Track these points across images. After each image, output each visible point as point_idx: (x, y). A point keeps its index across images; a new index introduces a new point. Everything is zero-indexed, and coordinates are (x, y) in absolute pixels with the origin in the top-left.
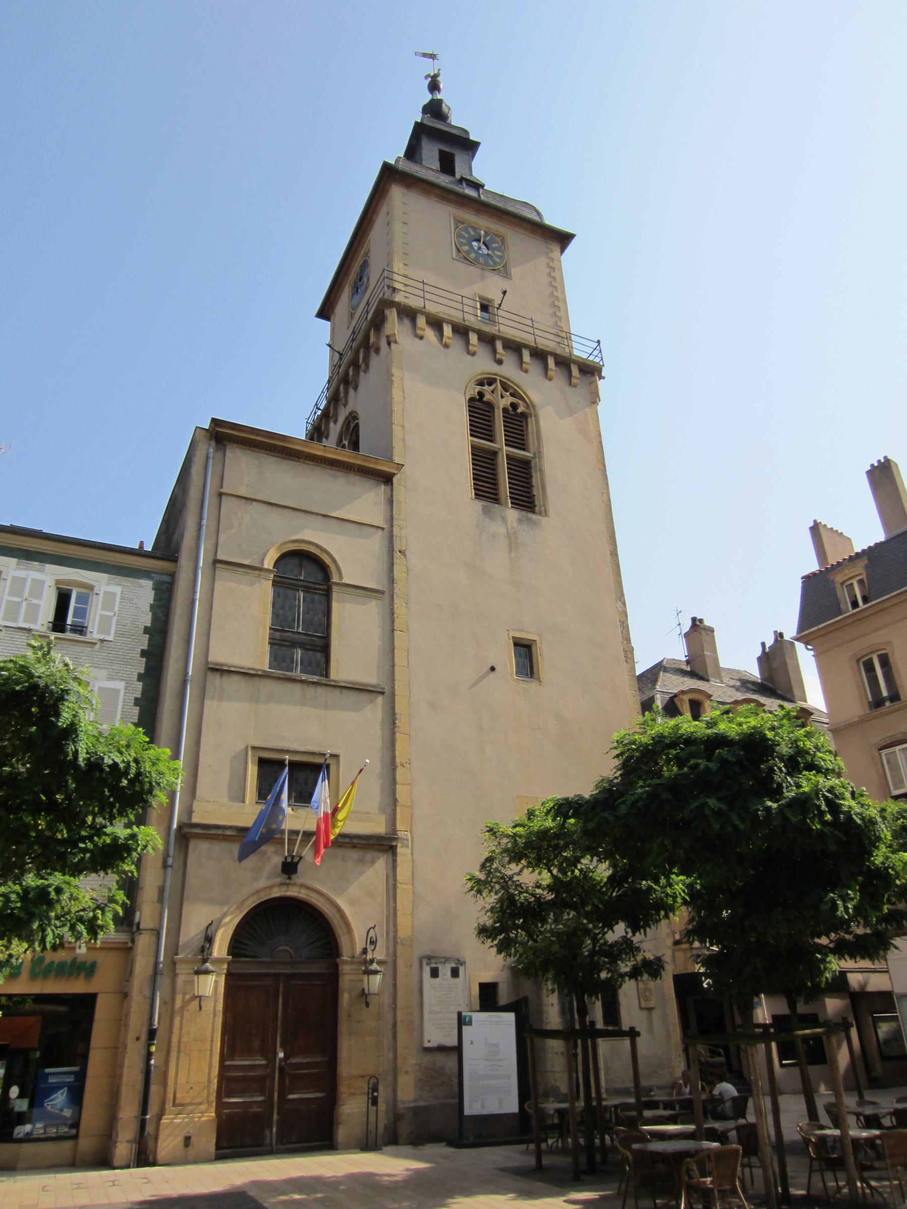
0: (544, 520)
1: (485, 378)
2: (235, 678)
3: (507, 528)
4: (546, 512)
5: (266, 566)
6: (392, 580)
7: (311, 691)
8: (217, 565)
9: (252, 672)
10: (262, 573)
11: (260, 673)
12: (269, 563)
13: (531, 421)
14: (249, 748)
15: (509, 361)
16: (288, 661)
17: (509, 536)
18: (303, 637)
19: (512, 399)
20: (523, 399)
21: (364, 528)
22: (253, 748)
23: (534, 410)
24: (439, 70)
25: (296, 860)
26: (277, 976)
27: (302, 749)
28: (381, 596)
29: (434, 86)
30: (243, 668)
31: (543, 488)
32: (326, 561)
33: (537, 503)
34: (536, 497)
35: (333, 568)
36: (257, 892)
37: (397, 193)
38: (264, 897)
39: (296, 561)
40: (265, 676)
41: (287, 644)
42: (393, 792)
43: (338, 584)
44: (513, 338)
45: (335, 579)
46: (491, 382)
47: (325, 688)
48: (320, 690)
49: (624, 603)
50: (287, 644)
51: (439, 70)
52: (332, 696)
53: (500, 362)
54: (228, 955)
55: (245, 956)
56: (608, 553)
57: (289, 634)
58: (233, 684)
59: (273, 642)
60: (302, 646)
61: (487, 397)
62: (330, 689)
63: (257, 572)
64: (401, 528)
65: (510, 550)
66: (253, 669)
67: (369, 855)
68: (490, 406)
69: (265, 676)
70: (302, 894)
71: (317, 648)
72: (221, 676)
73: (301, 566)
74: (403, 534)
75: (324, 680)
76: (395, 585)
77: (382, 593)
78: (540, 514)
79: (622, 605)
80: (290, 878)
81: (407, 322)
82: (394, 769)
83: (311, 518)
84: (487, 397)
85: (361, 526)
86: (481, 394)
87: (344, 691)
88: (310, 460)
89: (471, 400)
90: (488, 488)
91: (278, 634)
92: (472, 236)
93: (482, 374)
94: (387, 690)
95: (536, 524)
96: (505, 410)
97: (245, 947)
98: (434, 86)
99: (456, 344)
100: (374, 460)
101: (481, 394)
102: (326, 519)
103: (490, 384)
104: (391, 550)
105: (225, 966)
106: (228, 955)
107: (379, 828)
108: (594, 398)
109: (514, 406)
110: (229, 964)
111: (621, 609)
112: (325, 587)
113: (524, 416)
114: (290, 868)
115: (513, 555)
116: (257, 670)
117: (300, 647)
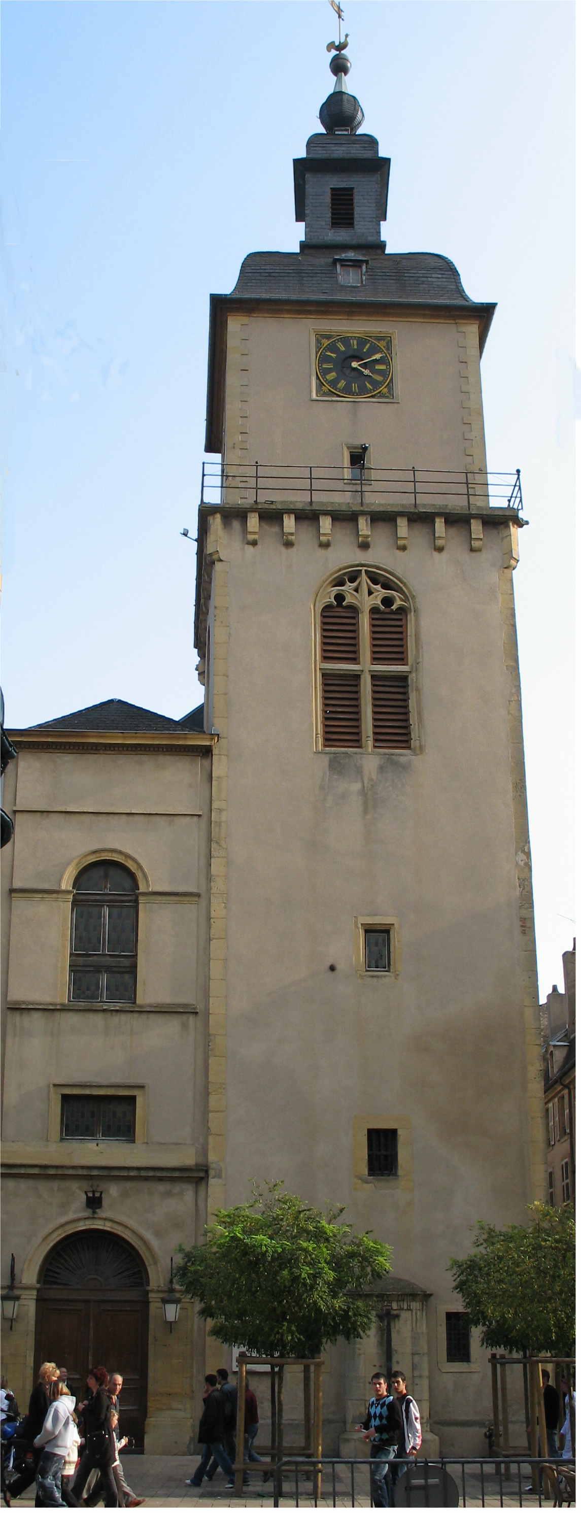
0: (416, 761)
1: (344, 574)
2: (36, 1015)
3: (363, 783)
4: (421, 747)
5: (63, 887)
6: (209, 878)
7: (116, 1019)
8: (13, 895)
9: (51, 1007)
10: (60, 896)
11: (58, 1007)
12: (66, 883)
13: (411, 617)
14: (51, 1086)
15: (380, 539)
16: (93, 988)
17: (363, 792)
18: (108, 958)
19: (381, 592)
20: (398, 590)
21: (176, 819)
22: (55, 1085)
23: (414, 603)
24: (347, 36)
25: (97, 1195)
26: (87, 1301)
27: (105, 1083)
28: (196, 899)
29: (339, 67)
30: (41, 1004)
31: (420, 714)
32: (131, 868)
33: (413, 736)
34: (412, 727)
35: (139, 876)
36: (62, 1226)
37: (234, 325)
38: (70, 1230)
39: (100, 872)
40: (64, 1009)
41: (92, 969)
42: (205, 1121)
43: (144, 894)
44: (382, 509)
45: (142, 888)
46: (353, 577)
47: (129, 1015)
48: (123, 1017)
49: (528, 854)
50: (92, 969)
51: (347, 36)
52: (135, 1021)
53: (365, 546)
54: (38, 1283)
55: (56, 1283)
56: (511, 786)
57: (95, 958)
58: (36, 1021)
59: (74, 968)
60: (109, 969)
61: (349, 600)
62: (136, 1015)
63: (55, 895)
64: (220, 810)
65: (365, 811)
66: (51, 1004)
67: (177, 1188)
68: (354, 610)
69: (64, 1009)
70: (107, 1227)
71: (124, 970)
72: (21, 1014)
73: (106, 876)
74: (224, 818)
75: (128, 1006)
76: (212, 884)
77: (198, 895)
78: (414, 751)
79: (525, 857)
80: (94, 1212)
81: (236, 524)
82: (206, 1093)
83: (114, 820)
84: (349, 600)
85: (172, 817)
86: (340, 598)
87: (152, 1016)
88: (110, 750)
89: (328, 608)
90: (393, 646)
91: (81, 960)
92: (343, 352)
93: (340, 570)
94: (200, 1007)
95: (405, 768)
96: (374, 610)
97: (56, 1275)
98: (339, 67)
99: (304, 537)
100: (183, 736)
101: (340, 598)
102: (131, 818)
103: (352, 580)
104: (210, 840)
105: (35, 1293)
106: (38, 1283)
107: (187, 1158)
108: (508, 562)
109: (388, 602)
110: (38, 1290)
111: (522, 863)
112: (133, 898)
113: (402, 610)
114: (94, 1203)
115: (368, 817)
116: (56, 1005)
117: (105, 972)
